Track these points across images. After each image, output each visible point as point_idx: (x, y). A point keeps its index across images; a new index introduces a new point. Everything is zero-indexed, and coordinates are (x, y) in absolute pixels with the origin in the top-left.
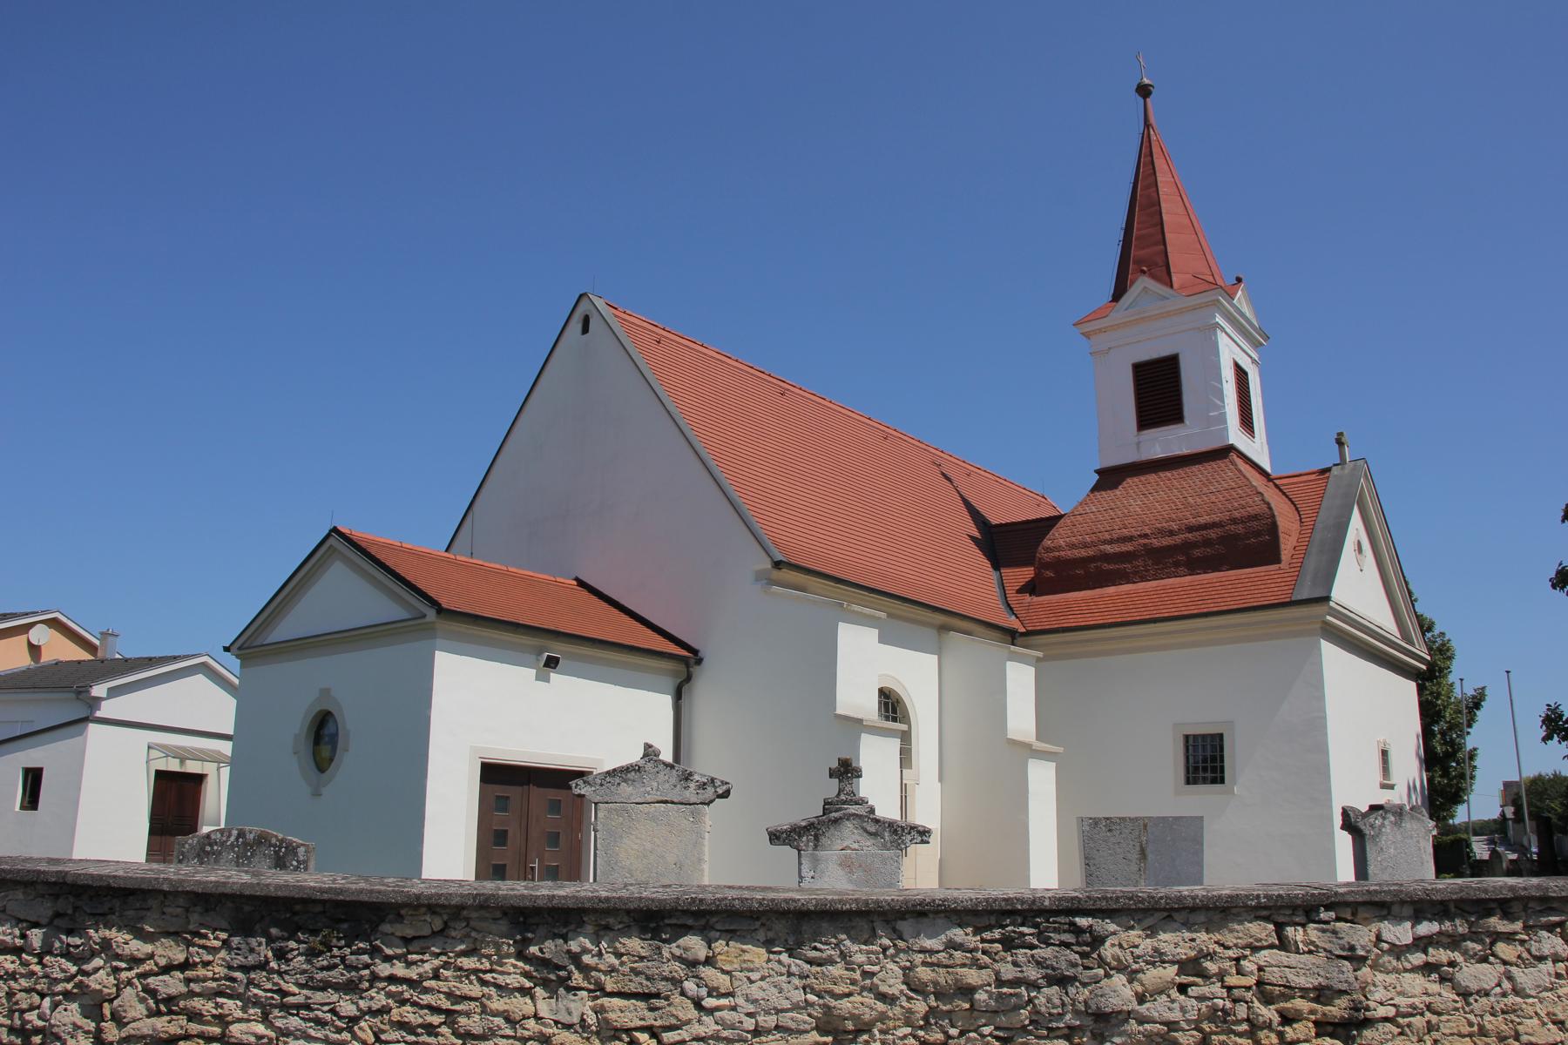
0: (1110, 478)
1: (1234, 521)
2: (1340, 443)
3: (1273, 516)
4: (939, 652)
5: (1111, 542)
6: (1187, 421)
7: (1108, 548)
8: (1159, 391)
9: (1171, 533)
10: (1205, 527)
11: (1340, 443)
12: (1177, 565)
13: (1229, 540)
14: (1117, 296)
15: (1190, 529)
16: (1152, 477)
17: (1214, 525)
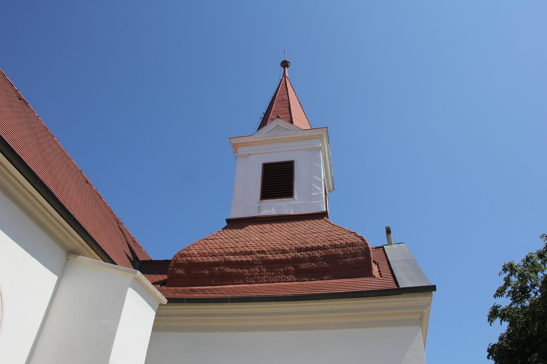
0: (234, 223)
1: (335, 246)
2: (388, 231)
3: (367, 244)
4: (61, 274)
5: (234, 254)
6: (296, 196)
7: (232, 258)
8: (278, 180)
9: (284, 252)
10: (312, 249)
11: (388, 231)
12: (287, 273)
13: (330, 258)
14: (264, 123)
15: (299, 250)
16: (267, 226)
17: (318, 248)
